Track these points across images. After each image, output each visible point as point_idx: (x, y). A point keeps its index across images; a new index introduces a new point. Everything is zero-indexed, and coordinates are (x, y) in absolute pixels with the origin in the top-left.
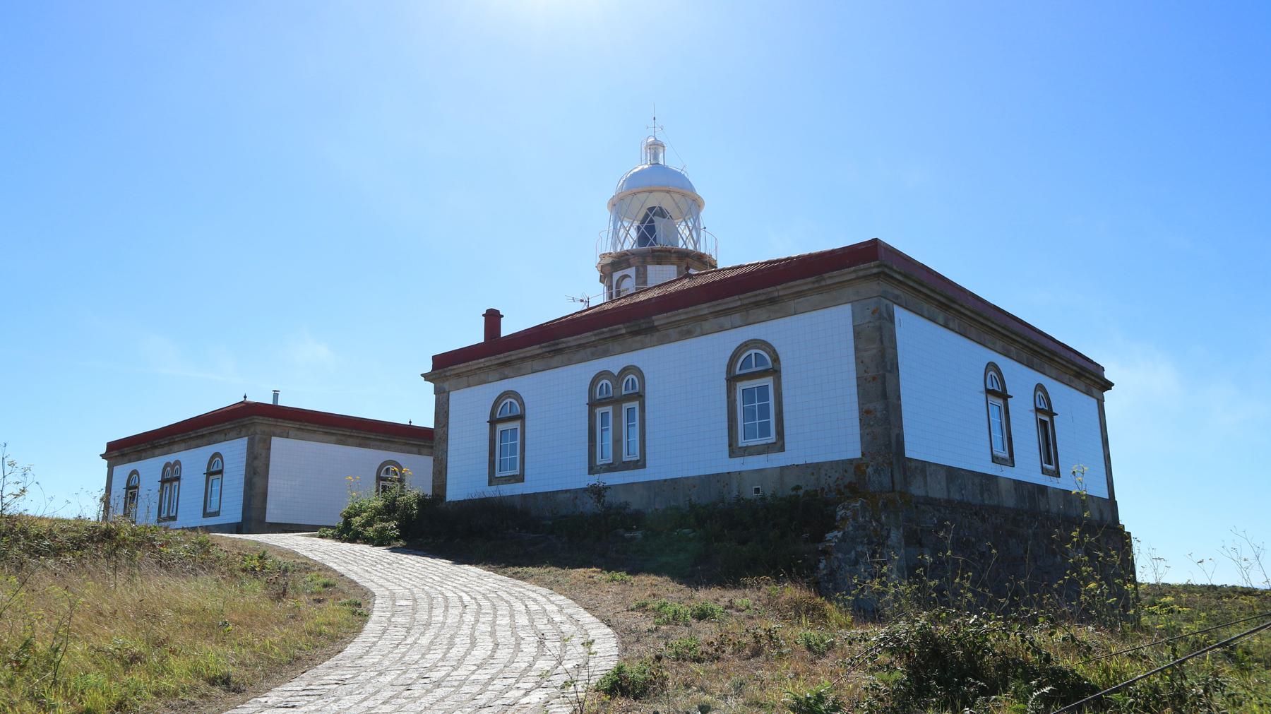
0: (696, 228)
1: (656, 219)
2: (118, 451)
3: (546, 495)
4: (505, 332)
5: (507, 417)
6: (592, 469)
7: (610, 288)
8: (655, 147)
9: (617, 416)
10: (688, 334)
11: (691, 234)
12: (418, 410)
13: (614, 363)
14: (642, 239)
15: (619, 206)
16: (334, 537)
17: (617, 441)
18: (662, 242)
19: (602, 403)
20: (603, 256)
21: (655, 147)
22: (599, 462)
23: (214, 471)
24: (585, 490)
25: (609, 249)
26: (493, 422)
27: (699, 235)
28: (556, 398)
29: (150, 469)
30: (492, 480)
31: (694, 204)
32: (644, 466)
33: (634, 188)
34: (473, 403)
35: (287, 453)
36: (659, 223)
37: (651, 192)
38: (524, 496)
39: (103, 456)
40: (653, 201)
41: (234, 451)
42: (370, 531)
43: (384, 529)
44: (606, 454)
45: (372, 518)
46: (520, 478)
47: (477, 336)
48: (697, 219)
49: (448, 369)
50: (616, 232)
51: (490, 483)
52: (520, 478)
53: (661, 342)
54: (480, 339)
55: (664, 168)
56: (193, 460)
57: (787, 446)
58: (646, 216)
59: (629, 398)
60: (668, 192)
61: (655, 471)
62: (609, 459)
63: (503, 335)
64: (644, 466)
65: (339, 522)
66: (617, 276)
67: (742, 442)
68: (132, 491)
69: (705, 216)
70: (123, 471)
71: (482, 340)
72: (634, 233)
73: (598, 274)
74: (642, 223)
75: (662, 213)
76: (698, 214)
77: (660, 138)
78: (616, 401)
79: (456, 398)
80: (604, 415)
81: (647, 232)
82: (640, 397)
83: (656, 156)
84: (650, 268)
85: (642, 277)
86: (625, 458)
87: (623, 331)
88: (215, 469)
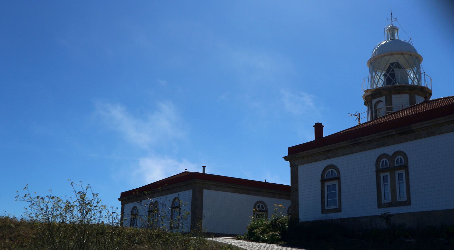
0: (418, 73)
1: (395, 69)
2: (126, 197)
3: (355, 219)
4: (325, 134)
5: (330, 178)
6: (380, 205)
7: (371, 108)
8: (393, 30)
9: (393, 178)
10: (432, 134)
11: (416, 76)
12: (281, 176)
13: (390, 150)
14: (388, 81)
15: (374, 64)
16: (245, 239)
17: (393, 191)
18: (399, 82)
19: (384, 170)
20: (366, 91)
21: (393, 30)
22: (383, 201)
23: (175, 206)
24: (380, 216)
25: (369, 88)
26: (323, 181)
27: (420, 77)
28: (356, 169)
29: (143, 207)
30: (324, 211)
31: (415, 60)
32: (410, 204)
33: (382, 53)
34: (312, 171)
35: (210, 196)
36: (397, 72)
37: (392, 55)
38: (341, 219)
39: (119, 199)
40: (393, 60)
41: (185, 197)
42: (266, 237)
43: (274, 235)
44: (387, 197)
45: (265, 230)
46: (339, 210)
47: (311, 137)
48: (419, 68)
49: (296, 154)
50: (373, 78)
51: (323, 212)
52: (339, 210)
53: (416, 138)
54: (311, 137)
55: (399, 41)
56: (165, 201)
57: (342, 211)
58: (389, 68)
59: (399, 168)
60: (402, 54)
61: (417, 206)
62: (389, 200)
63: (325, 135)
64: (410, 204)
65: (246, 232)
66: (374, 101)
67: (327, 208)
68: (134, 214)
69: (424, 65)
70: (129, 206)
71: (313, 139)
72: (383, 78)
73: (363, 101)
74: (388, 71)
75: (398, 66)
76: (419, 65)
77: (395, 24)
78: (392, 170)
79: (302, 169)
80: (385, 177)
81: (390, 77)
82: (405, 167)
83: (393, 35)
84: (393, 96)
85: (389, 102)
86: (399, 200)
87: (394, 133)
88: (176, 205)
